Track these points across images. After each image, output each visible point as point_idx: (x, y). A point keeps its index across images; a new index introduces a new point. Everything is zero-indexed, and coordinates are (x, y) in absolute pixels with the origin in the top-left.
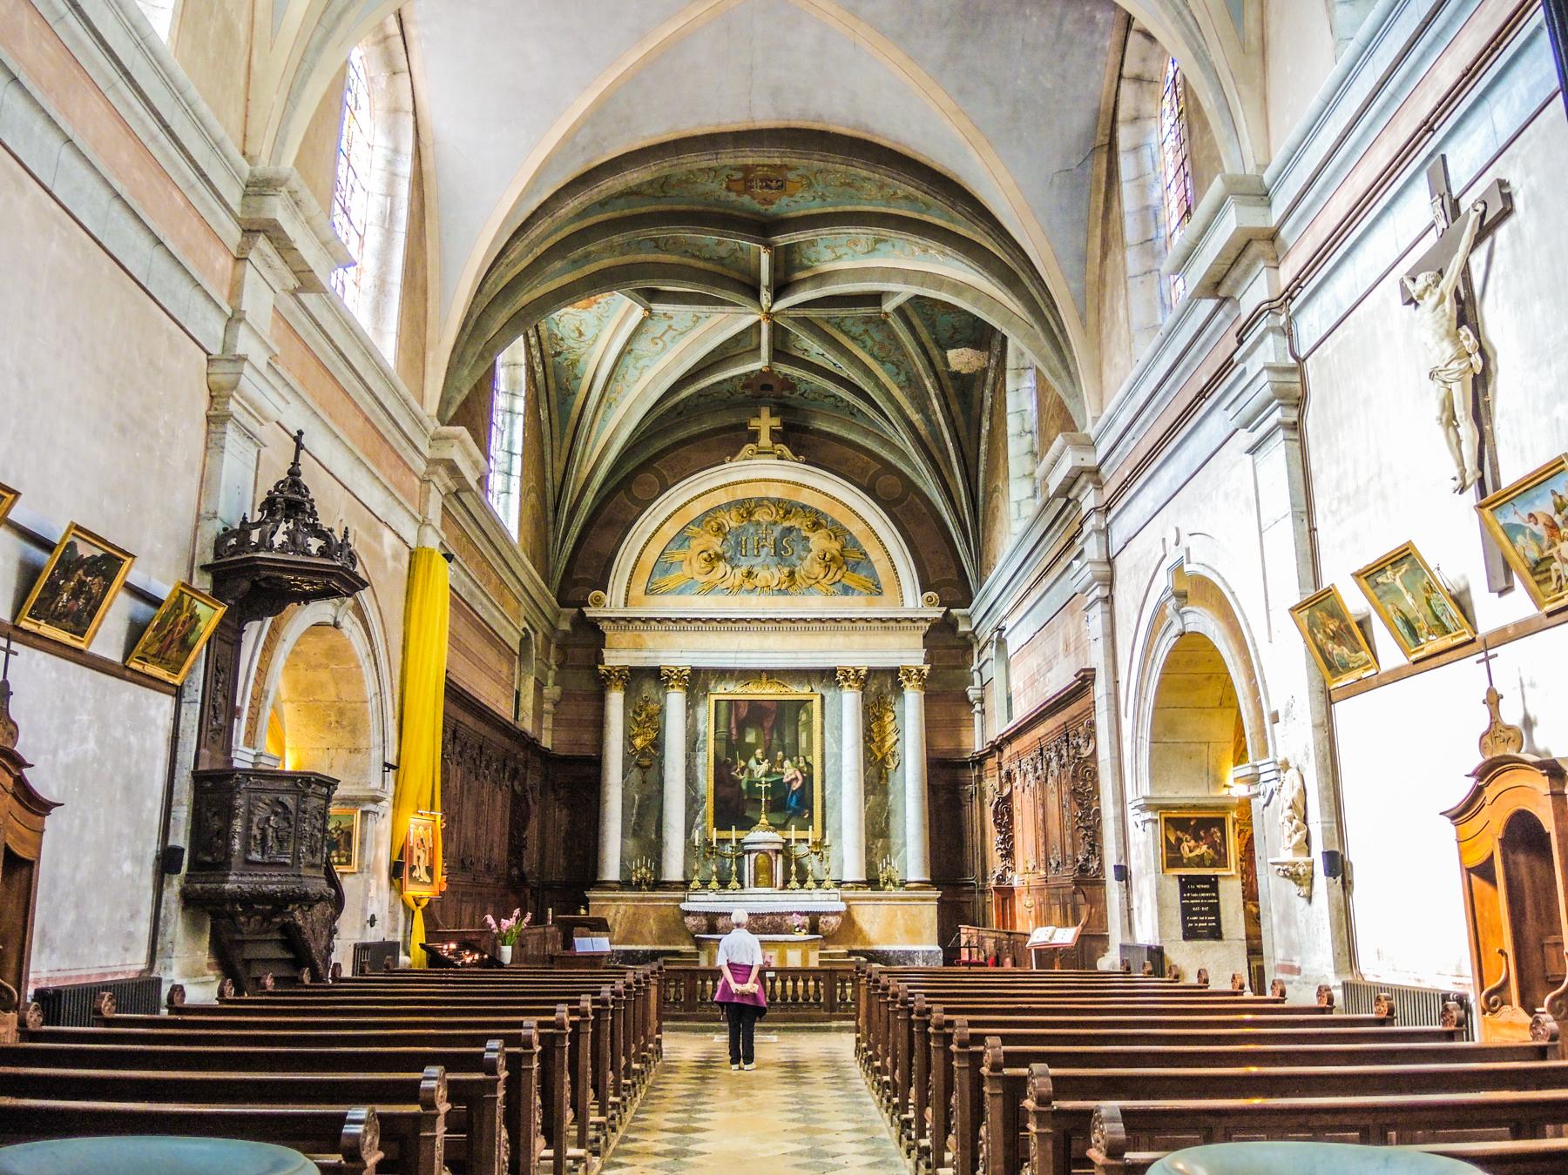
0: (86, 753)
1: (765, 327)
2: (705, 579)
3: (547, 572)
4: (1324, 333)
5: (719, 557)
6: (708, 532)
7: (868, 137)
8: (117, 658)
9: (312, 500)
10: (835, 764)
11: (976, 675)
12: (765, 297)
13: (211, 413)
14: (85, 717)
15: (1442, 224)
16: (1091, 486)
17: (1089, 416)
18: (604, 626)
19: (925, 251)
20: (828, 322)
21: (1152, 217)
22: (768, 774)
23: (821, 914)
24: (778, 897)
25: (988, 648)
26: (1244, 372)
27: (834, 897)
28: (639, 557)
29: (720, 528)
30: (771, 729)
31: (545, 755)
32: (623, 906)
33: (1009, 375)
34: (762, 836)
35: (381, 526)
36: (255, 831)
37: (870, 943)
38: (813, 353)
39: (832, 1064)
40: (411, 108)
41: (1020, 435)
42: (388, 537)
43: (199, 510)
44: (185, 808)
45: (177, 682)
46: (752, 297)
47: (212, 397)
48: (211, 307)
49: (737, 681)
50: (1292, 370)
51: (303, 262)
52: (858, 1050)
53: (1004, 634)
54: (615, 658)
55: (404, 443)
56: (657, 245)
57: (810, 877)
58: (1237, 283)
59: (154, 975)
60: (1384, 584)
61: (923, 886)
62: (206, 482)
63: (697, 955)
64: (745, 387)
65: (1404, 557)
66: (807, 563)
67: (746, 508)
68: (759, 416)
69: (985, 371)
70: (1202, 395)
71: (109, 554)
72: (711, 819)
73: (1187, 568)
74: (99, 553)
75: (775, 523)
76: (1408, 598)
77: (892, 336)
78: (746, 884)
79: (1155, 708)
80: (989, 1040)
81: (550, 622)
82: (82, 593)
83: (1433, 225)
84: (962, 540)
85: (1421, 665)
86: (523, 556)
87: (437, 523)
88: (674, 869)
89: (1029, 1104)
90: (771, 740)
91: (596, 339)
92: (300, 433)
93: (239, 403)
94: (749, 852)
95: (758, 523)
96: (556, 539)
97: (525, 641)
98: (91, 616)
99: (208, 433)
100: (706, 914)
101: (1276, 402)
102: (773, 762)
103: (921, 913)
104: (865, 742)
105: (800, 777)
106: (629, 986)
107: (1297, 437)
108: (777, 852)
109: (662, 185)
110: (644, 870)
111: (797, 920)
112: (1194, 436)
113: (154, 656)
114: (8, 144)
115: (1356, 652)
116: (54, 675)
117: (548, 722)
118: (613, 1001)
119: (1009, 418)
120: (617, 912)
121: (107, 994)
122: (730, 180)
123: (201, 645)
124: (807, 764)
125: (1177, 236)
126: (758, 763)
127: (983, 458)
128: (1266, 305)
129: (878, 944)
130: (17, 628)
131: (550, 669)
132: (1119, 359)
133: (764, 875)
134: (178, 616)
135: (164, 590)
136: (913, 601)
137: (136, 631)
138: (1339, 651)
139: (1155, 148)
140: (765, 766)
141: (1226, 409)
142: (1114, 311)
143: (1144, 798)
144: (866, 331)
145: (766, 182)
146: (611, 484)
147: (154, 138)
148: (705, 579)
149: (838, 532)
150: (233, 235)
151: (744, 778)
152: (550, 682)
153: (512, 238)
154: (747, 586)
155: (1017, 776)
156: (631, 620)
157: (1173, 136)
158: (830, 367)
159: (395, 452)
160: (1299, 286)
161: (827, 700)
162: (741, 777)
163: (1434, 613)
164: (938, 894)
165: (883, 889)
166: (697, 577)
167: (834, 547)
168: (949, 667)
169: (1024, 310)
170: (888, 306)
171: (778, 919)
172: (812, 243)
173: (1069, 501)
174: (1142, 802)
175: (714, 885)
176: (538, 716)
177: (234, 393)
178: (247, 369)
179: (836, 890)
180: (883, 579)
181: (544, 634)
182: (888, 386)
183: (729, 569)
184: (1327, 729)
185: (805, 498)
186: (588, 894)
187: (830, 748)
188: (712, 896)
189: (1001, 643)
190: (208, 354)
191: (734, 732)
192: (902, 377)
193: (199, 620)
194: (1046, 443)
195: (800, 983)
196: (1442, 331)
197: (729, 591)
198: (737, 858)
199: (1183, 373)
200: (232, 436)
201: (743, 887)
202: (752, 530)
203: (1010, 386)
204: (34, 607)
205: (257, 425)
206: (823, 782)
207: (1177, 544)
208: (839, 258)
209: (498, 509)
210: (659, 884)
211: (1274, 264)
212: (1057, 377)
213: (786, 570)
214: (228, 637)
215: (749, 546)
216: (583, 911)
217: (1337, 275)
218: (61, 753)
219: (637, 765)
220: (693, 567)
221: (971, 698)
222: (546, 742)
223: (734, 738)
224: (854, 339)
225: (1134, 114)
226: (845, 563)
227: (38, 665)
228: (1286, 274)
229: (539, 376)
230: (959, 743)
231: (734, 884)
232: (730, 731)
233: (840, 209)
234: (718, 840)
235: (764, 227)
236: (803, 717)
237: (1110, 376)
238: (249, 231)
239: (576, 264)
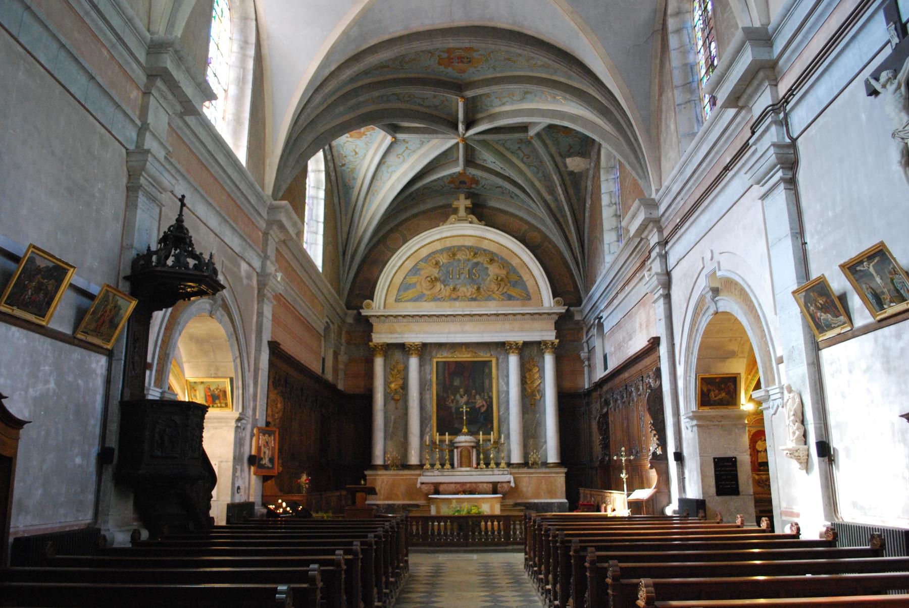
0: (48, 390)
1: (461, 146)
4: (810, 121)
5: (437, 279)
6: (430, 266)
7: (520, 30)
8: (67, 330)
9: (191, 237)
11: (585, 345)
12: (461, 127)
13: (129, 185)
14: (47, 368)
15: (896, 40)
16: (655, 230)
17: (653, 189)
18: (372, 320)
19: (554, 98)
20: (497, 143)
21: (689, 70)
22: (466, 403)
24: (474, 473)
25: (592, 329)
26: (756, 150)
27: (506, 472)
29: (437, 263)
31: (339, 392)
33: (602, 172)
34: (464, 440)
35: (239, 259)
36: (157, 437)
38: (489, 161)
39: (510, 570)
40: (254, 17)
41: (609, 206)
42: (244, 266)
43: (122, 242)
44: (116, 424)
45: (109, 347)
46: (455, 132)
47: (129, 175)
48: (128, 121)
50: (787, 146)
51: (185, 95)
52: (527, 565)
53: (602, 320)
54: (380, 337)
55: (252, 211)
56: (398, 97)
57: (492, 462)
58: (751, 96)
59: (97, 526)
60: (861, 271)
61: (557, 465)
62: (127, 226)
63: (429, 506)
64: (450, 182)
65: (879, 254)
67: (452, 252)
68: (458, 199)
69: (588, 170)
70: (727, 169)
71: (58, 266)
73: (719, 274)
74: (51, 265)
76: (878, 280)
77: (535, 151)
79: (698, 359)
80: (589, 549)
81: (340, 317)
82: (42, 289)
83: (889, 42)
84: (576, 268)
85: (884, 323)
86: (326, 281)
87: (273, 258)
88: (414, 460)
89: (587, 564)
91: (365, 155)
92: (183, 196)
93: (146, 179)
95: (459, 260)
96: (344, 271)
97: (327, 328)
98: (49, 304)
99: (127, 197)
100: (432, 483)
101: (779, 166)
102: (470, 396)
105: (485, 404)
106: (386, 531)
107: (792, 187)
108: (473, 447)
109: (401, 61)
111: (159, 245)
112: (722, 194)
113: (92, 331)
114: (6, 26)
115: (837, 317)
116: (25, 341)
117: (341, 375)
118: (376, 542)
119: (603, 196)
121: (50, 543)
122: (440, 58)
123: (123, 323)
125: (705, 80)
127: (587, 221)
128: (770, 108)
130: (75, 338)
132: (672, 154)
133: (466, 461)
134: (106, 306)
135: (95, 289)
136: (547, 300)
137: (80, 314)
138: (823, 316)
139: (690, 31)
140: (465, 398)
141: (746, 173)
142: (668, 126)
143: (693, 412)
144: (519, 148)
145: (461, 59)
146: (375, 240)
147: (87, 13)
149: (505, 264)
150: (140, 77)
151: (453, 405)
152: (342, 353)
153: (314, 93)
155: (611, 402)
156: (387, 317)
157: (701, 22)
158: (499, 170)
159: (247, 216)
160: (792, 94)
161: (500, 360)
162: (452, 405)
163: (895, 287)
164: (565, 470)
167: (503, 273)
169: (614, 130)
170: (532, 132)
171: (474, 485)
172: (488, 95)
173: (642, 239)
174: (691, 414)
175: (438, 466)
176: (335, 371)
177: (143, 173)
178: (150, 158)
180: (531, 291)
181: (338, 325)
182: (532, 180)
183: (443, 287)
184: (816, 366)
185: (485, 245)
186: (366, 473)
188: (436, 473)
189: (601, 326)
190: (127, 149)
192: (540, 175)
193: (120, 309)
194: (627, 208)
195: (489, 523)
196: (900, 106)
199: (714, 157)
200: (142, 199)
202: (455, 264)
203: (603, 178)
204: (8, 298)
205: (159, 194)
207: (712, 259)
208: (504, 104)
209: (310, 252)
210: (406, 467)
211: (775, 83)
212: (633, 168)
213: (475, 287)
214: (141, 320)
215: (454, 273)
216: (363, 482)
217: (818, 84)
218: (31, 390)
219: (393, 399)
220: (423, 287)
221: (582, 358)
222: (340, 386)
224: (512, 153)
225: (677, 10)
226: (509, 282)
227: (13, 335)
228: (783, 88)
229: (333, 178)
231: (448, 466)
233: (504, 74)
235: (459, 87)
236: (487, 370)
237: (665, 165)
238: (152, 76)
239: (352, 108)
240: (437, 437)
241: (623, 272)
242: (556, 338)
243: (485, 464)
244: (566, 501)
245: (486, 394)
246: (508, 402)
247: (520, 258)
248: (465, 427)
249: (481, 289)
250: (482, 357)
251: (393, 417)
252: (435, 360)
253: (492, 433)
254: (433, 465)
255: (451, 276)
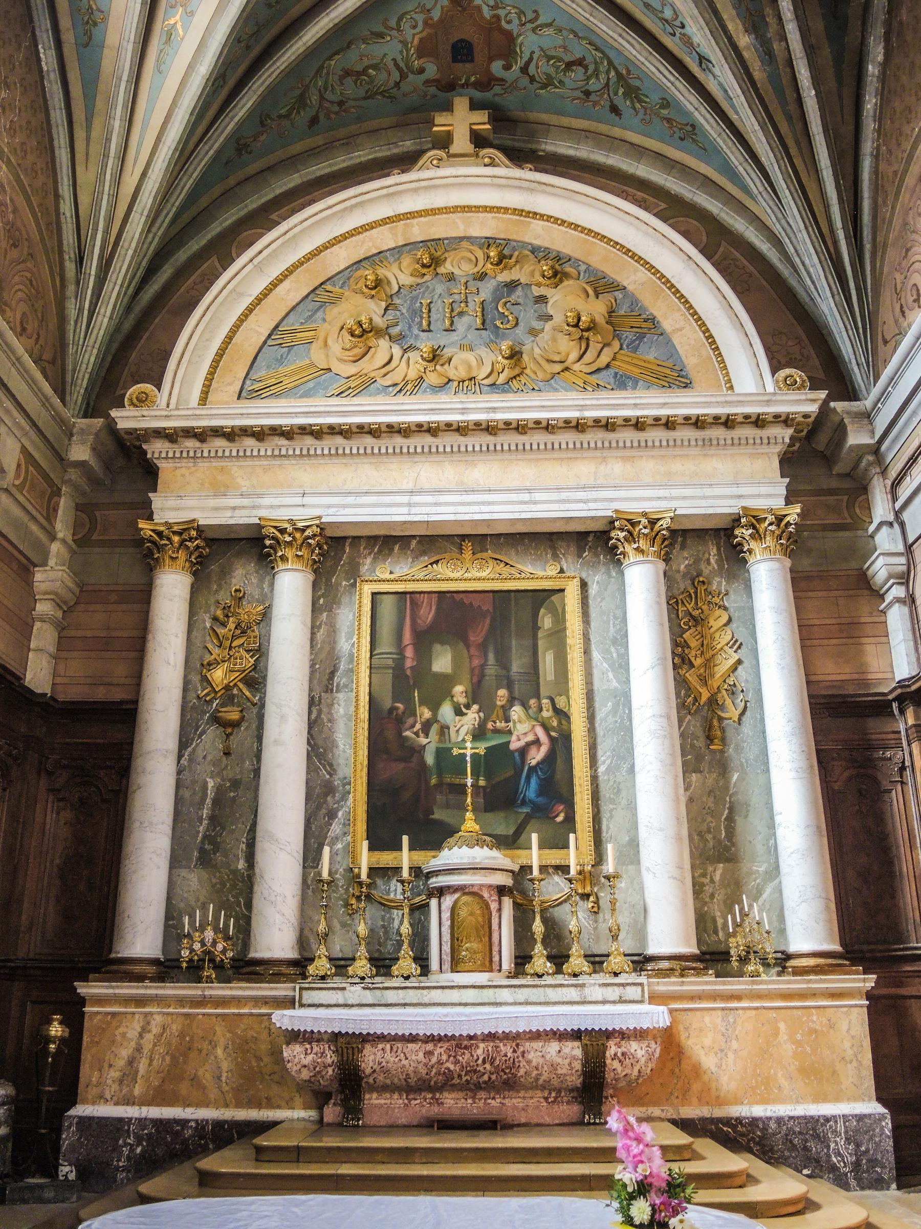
2: (352, 369)
3: (64, 383)
10: (614, 711)
18: (156, 449)
22: (479, 734)
23: (608, 1034)
24: (505, 995)
27: (633, 993)
28: (229, 339)
30: (483, 647)
32: (158, 1016)
37: (720, 1102)
49: (416, 558)
57: (575, 950)
66: (545, 336)
72: (361, 827)
75: (482, 277)
78: (434, 965)
90: (483, 666)
94: (441, 892)
95: (451, 278)
96: (81, 310)
100: (336, 1037)
101: (892, 581)
102: (487, 709)
103: (832, 1026)
104: (675, 666)
108: (502, 891)
110: (209, 934)
120: (144, 1030)
124: (557, 711)
126: (459, 712)
129: (738, 1101)
131: (53, 537)
140: (472, 717)
146: (186, 218)
148: (352, 369)
151: (430, 743)
154: (433, 379)
161: (593, 590)
162: (423, 740)
164: (869, 981)
165: (741, 974)
166: (337, 367)
168: (825, 528)
171: (506, 1049)
175: (362, 966)
179: (633, 978)
180: (690, 361)
183: (397, 351)
186: (84, 989)
187: (605, 679)
188: (355, 993)
191: (409, 652)
197: (401, 388)
198: (414, 909)
201: (425, 970)
206: (593, 748)
216: (56, 1030)
219: (216, 719)
223: (409, 663)
230: (862, 669)
231: (406, 964)
232: (401, 651)
234: (372, 871)
236: (546, 622)
240: (365, 859)
241: (906, 424)
242: (788, 501)
243: (550, 958)
244: (877, 1108)
245: (545, 702)
246: (628, 731)
247: (651, 268)
248: (469, 815)
249: (525, 357)
250: (532, 577)
251: (211, 784)
252: (367, 589)
253: (572, 836)
254: (341, 965)
255: (425, 323)
